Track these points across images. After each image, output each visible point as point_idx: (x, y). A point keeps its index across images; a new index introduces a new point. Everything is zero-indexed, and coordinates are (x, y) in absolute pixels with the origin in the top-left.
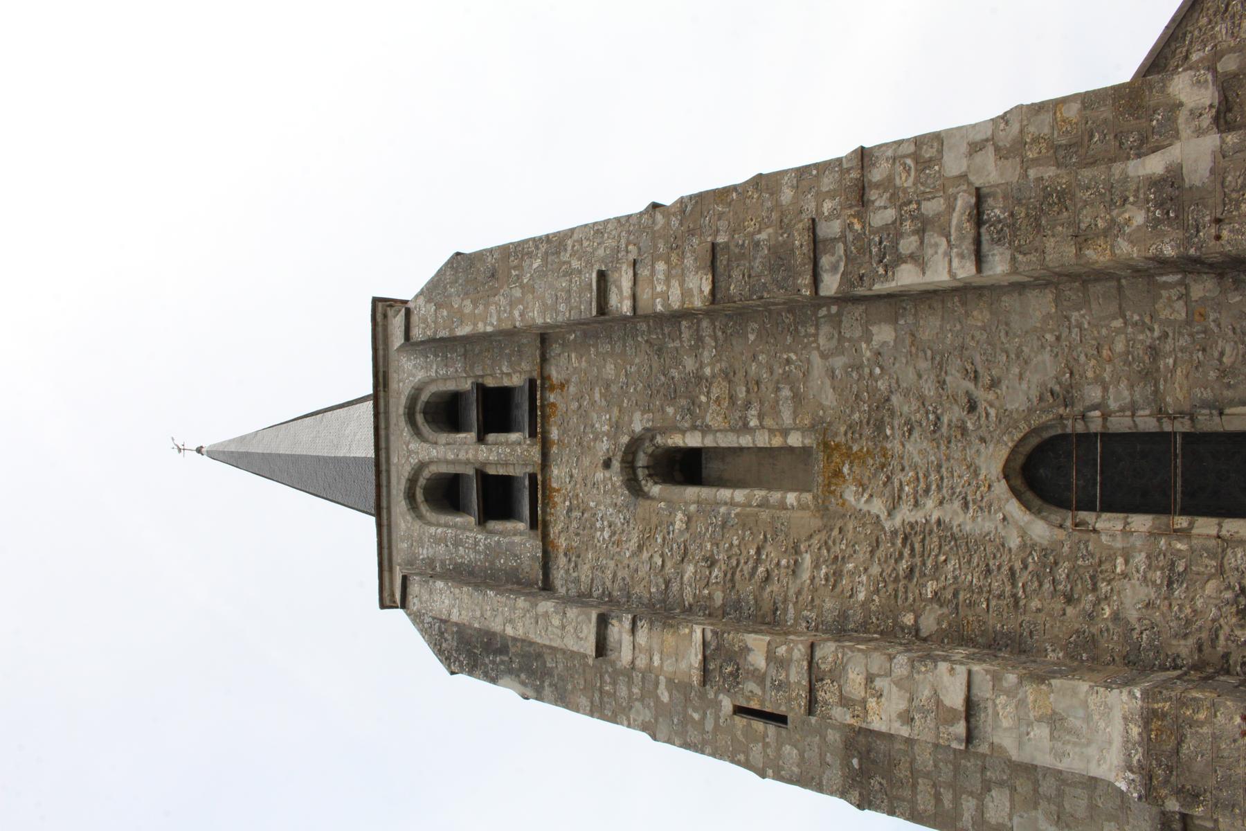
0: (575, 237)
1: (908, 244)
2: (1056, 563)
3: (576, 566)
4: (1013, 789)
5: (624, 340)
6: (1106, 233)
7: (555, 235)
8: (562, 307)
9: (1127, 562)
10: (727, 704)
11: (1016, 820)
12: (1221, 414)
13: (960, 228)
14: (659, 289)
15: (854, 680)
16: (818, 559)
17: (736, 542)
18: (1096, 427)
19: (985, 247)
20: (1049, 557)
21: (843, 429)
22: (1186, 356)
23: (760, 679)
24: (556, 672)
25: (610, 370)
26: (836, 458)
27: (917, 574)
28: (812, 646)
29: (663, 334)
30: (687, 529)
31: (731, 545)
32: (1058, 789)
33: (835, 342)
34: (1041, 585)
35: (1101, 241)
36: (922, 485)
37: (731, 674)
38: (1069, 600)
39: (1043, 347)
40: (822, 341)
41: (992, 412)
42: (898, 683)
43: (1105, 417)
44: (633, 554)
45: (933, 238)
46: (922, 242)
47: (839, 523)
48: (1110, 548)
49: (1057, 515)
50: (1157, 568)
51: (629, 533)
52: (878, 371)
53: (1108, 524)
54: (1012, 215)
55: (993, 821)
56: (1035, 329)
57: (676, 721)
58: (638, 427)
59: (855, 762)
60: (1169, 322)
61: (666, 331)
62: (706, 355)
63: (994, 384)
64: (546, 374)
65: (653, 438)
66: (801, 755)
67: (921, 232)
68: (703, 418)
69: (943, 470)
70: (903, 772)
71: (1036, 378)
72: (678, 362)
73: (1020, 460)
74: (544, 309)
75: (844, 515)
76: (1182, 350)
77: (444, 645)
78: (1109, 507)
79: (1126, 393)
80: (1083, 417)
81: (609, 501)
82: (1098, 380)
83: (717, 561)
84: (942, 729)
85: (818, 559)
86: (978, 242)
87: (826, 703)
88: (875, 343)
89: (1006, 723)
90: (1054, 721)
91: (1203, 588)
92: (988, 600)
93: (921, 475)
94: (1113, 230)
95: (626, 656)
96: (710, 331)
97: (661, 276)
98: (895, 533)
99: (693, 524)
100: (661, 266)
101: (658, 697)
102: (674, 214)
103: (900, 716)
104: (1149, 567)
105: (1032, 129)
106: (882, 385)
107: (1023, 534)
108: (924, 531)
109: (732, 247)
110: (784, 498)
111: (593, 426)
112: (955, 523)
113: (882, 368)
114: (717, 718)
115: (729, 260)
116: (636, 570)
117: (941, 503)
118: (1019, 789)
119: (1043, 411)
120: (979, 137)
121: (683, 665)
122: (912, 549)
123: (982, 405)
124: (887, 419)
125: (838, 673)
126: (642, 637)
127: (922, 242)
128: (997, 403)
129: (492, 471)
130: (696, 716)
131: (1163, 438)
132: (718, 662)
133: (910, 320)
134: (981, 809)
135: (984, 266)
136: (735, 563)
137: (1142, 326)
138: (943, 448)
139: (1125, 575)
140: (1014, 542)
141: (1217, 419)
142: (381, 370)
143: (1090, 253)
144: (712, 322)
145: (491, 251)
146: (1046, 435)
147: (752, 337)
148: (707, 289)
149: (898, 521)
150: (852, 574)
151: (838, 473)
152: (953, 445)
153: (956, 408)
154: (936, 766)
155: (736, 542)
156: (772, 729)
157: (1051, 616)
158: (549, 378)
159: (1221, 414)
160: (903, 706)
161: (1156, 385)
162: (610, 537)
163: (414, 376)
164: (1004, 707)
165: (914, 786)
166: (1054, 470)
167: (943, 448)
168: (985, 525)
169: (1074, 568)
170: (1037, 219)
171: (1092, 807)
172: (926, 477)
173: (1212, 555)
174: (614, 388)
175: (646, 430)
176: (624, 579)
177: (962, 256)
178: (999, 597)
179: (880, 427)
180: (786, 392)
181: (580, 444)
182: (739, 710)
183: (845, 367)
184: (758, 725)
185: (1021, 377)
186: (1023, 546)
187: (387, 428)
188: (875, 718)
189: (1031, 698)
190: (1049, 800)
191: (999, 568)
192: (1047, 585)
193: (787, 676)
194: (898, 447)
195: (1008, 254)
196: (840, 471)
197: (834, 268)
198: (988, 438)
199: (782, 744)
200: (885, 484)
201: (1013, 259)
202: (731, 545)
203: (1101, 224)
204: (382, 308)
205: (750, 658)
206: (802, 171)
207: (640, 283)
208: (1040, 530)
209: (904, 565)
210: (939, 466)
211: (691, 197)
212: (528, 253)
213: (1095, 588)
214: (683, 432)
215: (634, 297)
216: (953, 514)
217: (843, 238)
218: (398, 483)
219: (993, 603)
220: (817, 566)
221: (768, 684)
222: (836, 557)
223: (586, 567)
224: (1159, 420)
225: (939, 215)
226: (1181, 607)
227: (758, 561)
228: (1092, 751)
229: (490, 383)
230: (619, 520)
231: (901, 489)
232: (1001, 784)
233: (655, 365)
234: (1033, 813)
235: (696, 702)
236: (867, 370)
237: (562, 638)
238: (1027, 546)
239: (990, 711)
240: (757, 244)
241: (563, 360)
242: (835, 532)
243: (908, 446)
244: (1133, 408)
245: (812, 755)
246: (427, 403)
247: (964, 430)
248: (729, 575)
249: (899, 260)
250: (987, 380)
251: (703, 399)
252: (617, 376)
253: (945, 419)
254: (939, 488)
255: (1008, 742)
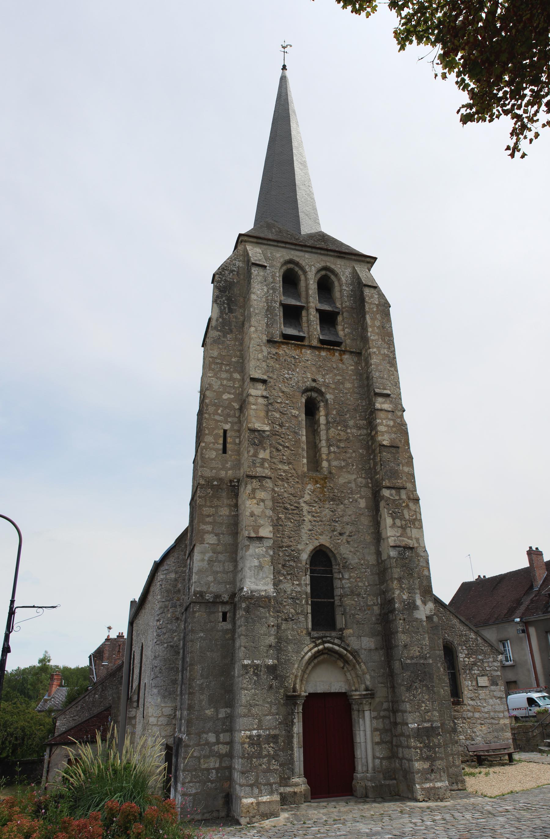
0: (395, 372)
1: (398, 522)
2: (295, 561)
3: (272, 358)
4: (218, 545)
5: (359, 394)
6: (401, 587)
7: (396, 362)
8: (377, 374)
9: (297, 585)
10: (227, 427)
11: (207, 545)
12: (342, 614)
13: (403, 541)
14: (384, 421)
15: (261, 494)
16: (287, 472)
17: (290, 437)
18: (336, 575)
19: (398, 549)
20: (297, 559)
21: (332, 485)
22: (358, 604)
23: (255, 455)
24: (225, 339)
25: (348, 385)
26: (322, 482)
27: (286, 511)
28: (271, 478)
29: (361, 412)
30: (293, 416)
31: (289, 435)
32: (221, 561)
33: (360, 484)
34: (287, 556)
35: (399, 585)
36: (316, 515)
37: (255, 442)
38: (284, 566)
39: (359, 560)
40: (360, 479)
41: (339, 541)
42: (263, 512)
43: (340, 579)
44: (280, 388)
45: (400, 531)
46: (399, 527)
47: (300, 482)
48: (301, 579)
49: (308, 562)
50: (296, 594)
51: (288, 387)
52: (351, 500)
53: (307, 579)
54: (407, 558)
55: (205, 537)
56: (365, 557)
57: (216, 401)
58: (328, 396)
59: (215, 483)
60: (367, 599)
61: (362, 414)
62: (354, 431)
63: (348, 542)
64: (346, 353)
65: (323, 401)
66: (213, 459)
67: (402, 527)
68: (332, 427)
69: (320, 523)
70: (216, 502)
71: (350, 556)
72: (352, 417)
73: (324, 549)
74: (377, 365)
75: (303, 484)
76: (360, 603)
77: (227, 272)
78: (311, 577)
79: (347, 586)
80: (340, 572)
81: (300, 379)
82: (350, 577)
83: (282, 428)
84: (251, 527)
85: (287, 472)
86: (399, 547)
87: (252, 483)
88: (359, 500)
89: (257, 550)
90: (260, 567)
91: (292, 608)
92: (280, 537)
93: (318, 514)
94: (402, 589)
95: (253, 392)
96: (363, 433)
97: (388, 423)
98: (299, 503)
99: (294, 419)
100: (391, 423)
101: (224, 393)
102: (401, 421)
103: (252, 512)
104: (296, 592)
105: (422, 559)
106: (346, 502)
107: (303, 550)
108: (301, 515)
109: (398, 455)
110: (303, 457)
111: (327, 374)
112: (304, 526)
113: (352, 502)
114: (221, 422)
115: (394, 453)
116: (274, 389)
117: (310, 521)
118: (218, 547)
119: (341, 559)
120: (420, 541)
121: (254, 420)
122: (294, 510)
123: (341, 537)
124: (335, 502)
125: (263, 488)
126: (261, 401)
127: (399, 527)
128: (342, 543)
129: (304, 313)
130: (219, 411)
131: (333, 597)
132: (258, 437)
133: (367, 514)
134: (208, 532)
135: (392, 548)
136: (282, 436)
137: (366, 591)
138: (328, 523)
139: (293, 584)
140: (300, 547)
141: (341, 613)
142: (346, 256)
143: (396, 582)
144: (366, 435)
145: (391, 327)
146: (332, 559)
147: (361, 451)
148: (385, 443)
149: (303, 505)
150: (283, 485)
151: (317, 482)
152: (329, 527)
153: (340, 528)
154: (221, 515)
155: (290, 437)
156: (221, 447)
157: (278, 559)
158: (344, 354)
159: (342, 614)
160: (256, 513)
161: (350, 595)
162: (286, 377)
163: (343, 275)
164: (262, 550)
165: (211, 507)
166: (322, 558)
167: (328, 523)
168: (305, 537)
169: (294, 568)
170: (405, 566)
171: (217, 572)
172: (318, 516)
173: (302, 611)
174: (341, 386)
175: (327, 400)
176: (270, 382)
177: (395, 541)
178: (282, 541)
179: (333, 500)
180: (343, 464)
181: (320, 367)
182: (225, 432)
183: (351, 488)
184: (221, 441)
185: (350, 551)
186: (299, 550)
187: (321, 254)
188: (250, 502)
189: (266, 559)
190: (217, 557)
191: (291, 541)
192: (287, 558)
193: (258, 467)
194: (327, 506)
195: (395, 556)
196: (318, 483)
197: (391, 495)
198: (332, 539)
199: (216, 451)
200: (314, 500)
201: (394, 558)
202: (289, 435)
203: (403, 585)
204: (369, 261)
205: (262, 451)
206: (413, 475)
207: (386, 413)
208: (305, 556)
209: (289, 506)
210: (322, 521)
211: (407, 429)
212: (389, 347)
213: (288, 574)
214: (327, 415)
215: (381, 410)
216: (307, 526)
217: (400, 499)
218: (297, 256)
219: (280, 539)
220: (285, 471)
221: (254, 458)
222: (288, 480)
223: (272, 363)
224: (340, 596)
225: (407, 534)
226: (285, 602)
227: (284, 447)
228: (253, 580)
229: (340, 318)
230: (292, 382)
231: (313, 506)
232: (219, 540)
233: (350, 407)
234: (211, 552)
235: (225, 412)
236: (351, 496)
237: (254, 359)
238: (299, 552)
239: (260, 545)
240: (399, 465)
241: (351, 362)
242: (297, 480)
243: (327, 510)
244: (343, 588)
245: (214, 464)
246: (329, 278)
247: (333, 531)
248: (277, 433)
249: (394, 519)
250: (349, 540)
251: (339, 428)
252: (346, 389)
253: (336, 524)
254: (315, 521)
255: (251, 551)
